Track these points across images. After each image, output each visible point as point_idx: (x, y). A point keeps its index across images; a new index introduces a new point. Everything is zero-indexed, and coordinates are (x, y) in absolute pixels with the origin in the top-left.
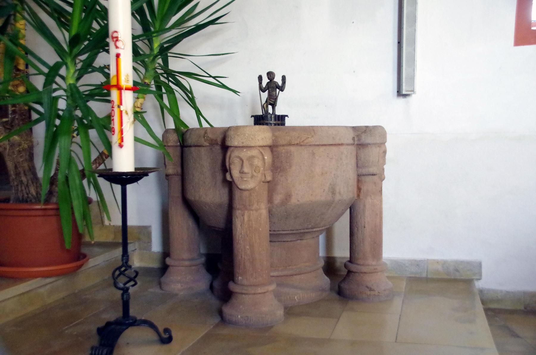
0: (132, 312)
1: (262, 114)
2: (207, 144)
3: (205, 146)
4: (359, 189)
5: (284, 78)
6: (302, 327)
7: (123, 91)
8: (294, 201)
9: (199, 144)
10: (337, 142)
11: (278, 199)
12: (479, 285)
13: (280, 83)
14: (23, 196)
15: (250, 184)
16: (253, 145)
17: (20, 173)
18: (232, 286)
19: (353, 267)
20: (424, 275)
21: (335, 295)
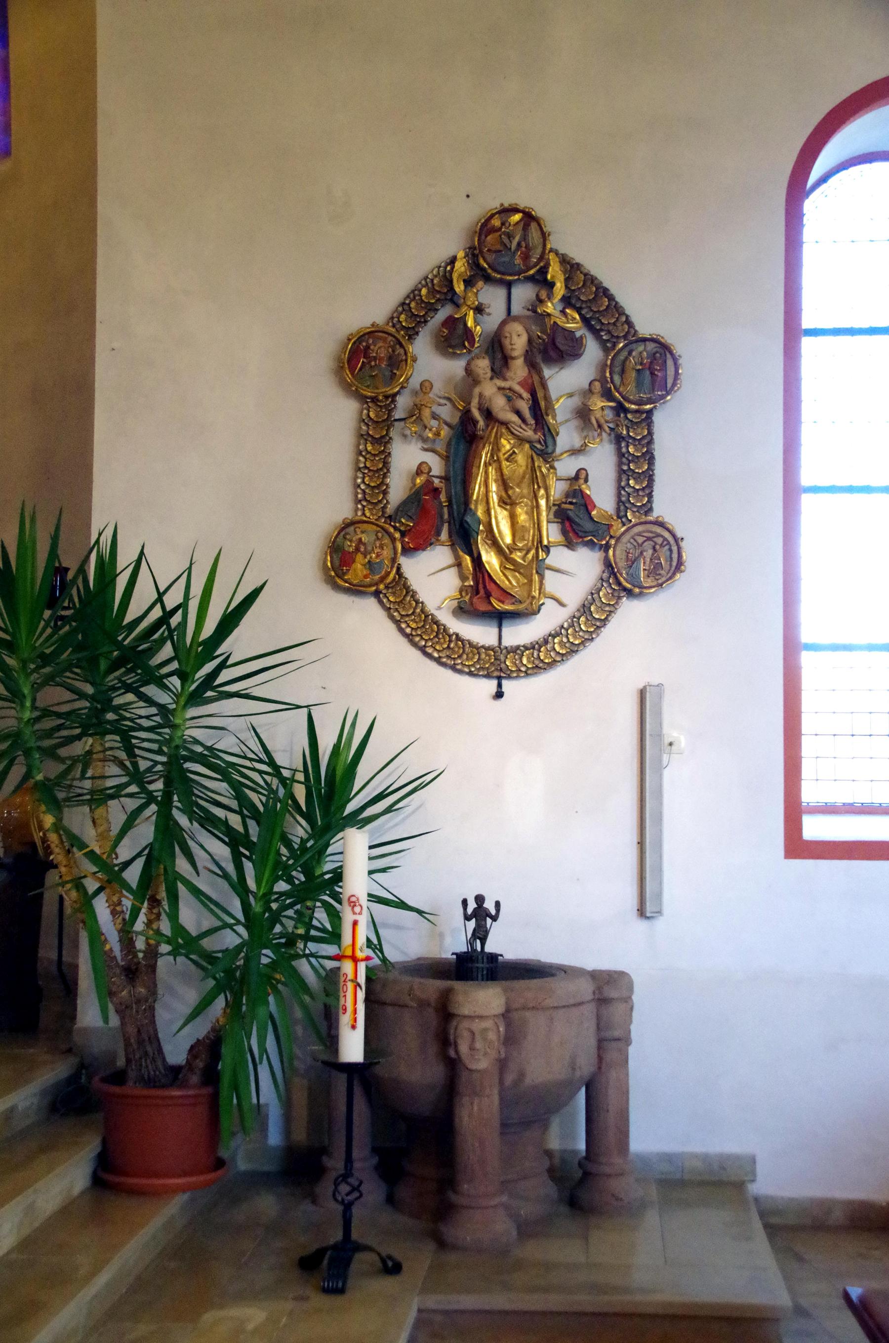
0: (355, 1235)
1: (466, 950)
4: (600, 1059)
5: (498, 904)
8: (528, 1081)
10: (578, 1000)
11: (509, 1079)
13: (493, 912)
19: (591, 1167)
20: (678, 1176)
21: (564, 1209)
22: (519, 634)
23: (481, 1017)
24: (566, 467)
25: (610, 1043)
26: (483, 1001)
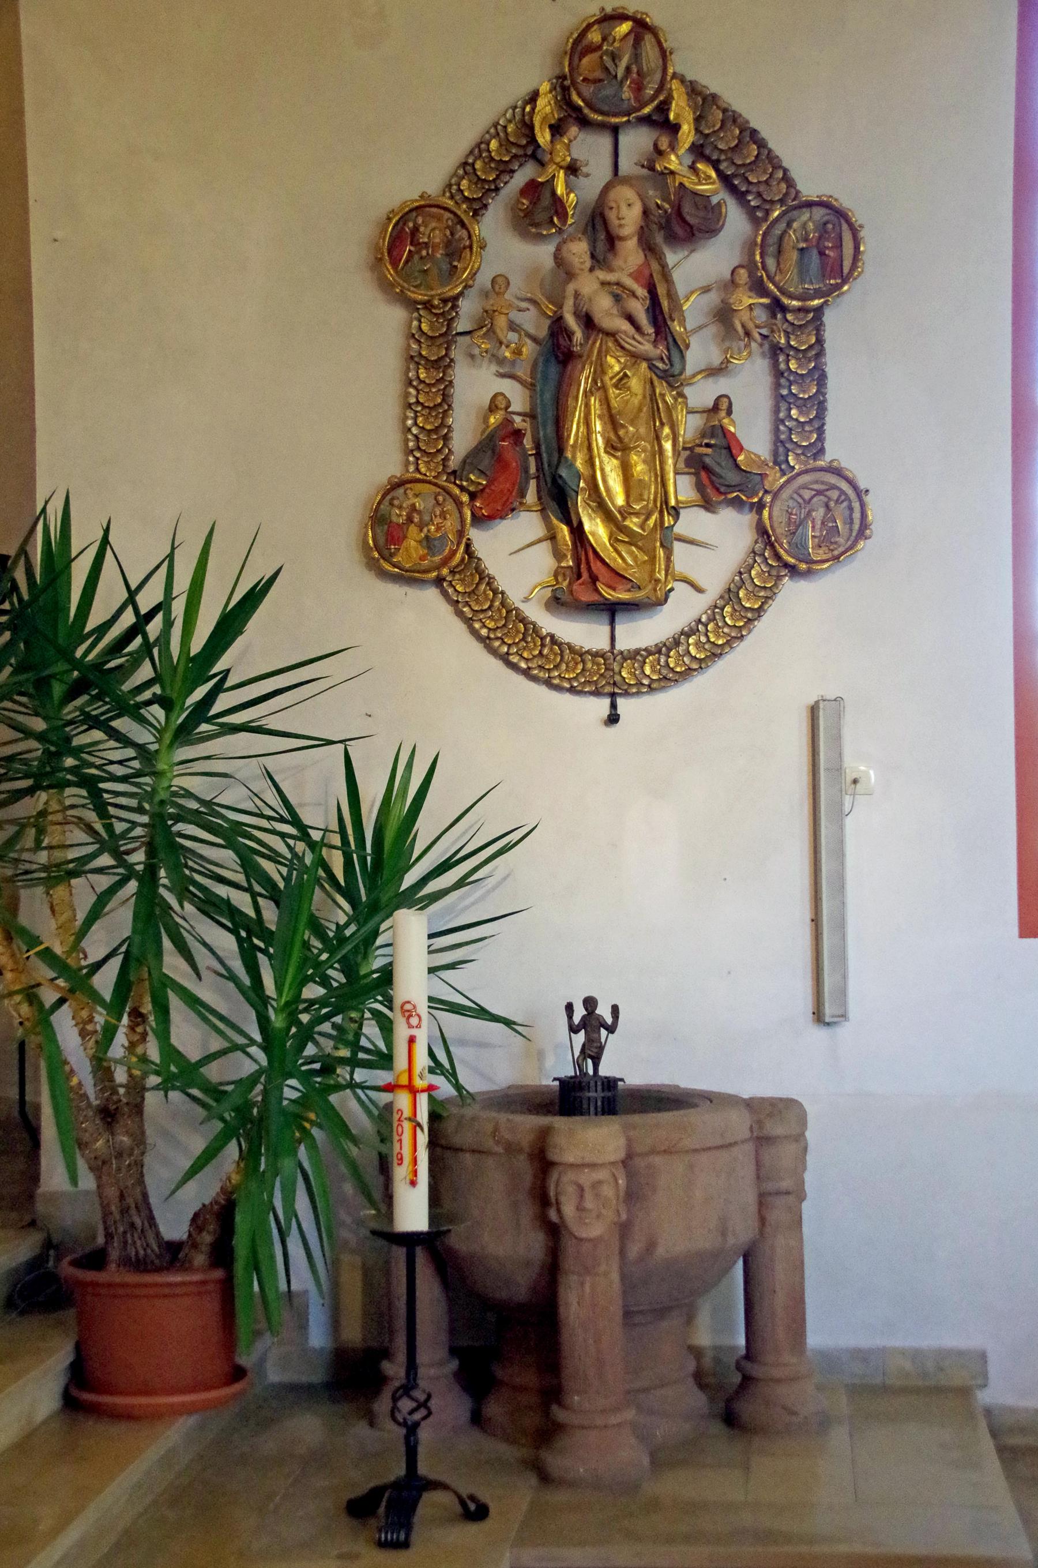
1: (573, 1074)
2: (500, 1149)
3: (496, 1154)
4: (762, 1220)
5: (615, 1010)
6: (675, 1485)
7: (418, 1095)
8: (660, 1251)
9: (481, 1149)
11: (634, 1250)
12: (984, 1397)
13: (609, 1020)
14: (137, 1253)
15: (595, 1230)
16: (600, 1162)
17: (129, 1208)
18: (560, 1415)
20: (878, 1380)
21: (717, 1428)
22: (638, 633)
23: (593, 1166)
24: (701, 393)
25: (776, 1199)
26: (592, 1144)
